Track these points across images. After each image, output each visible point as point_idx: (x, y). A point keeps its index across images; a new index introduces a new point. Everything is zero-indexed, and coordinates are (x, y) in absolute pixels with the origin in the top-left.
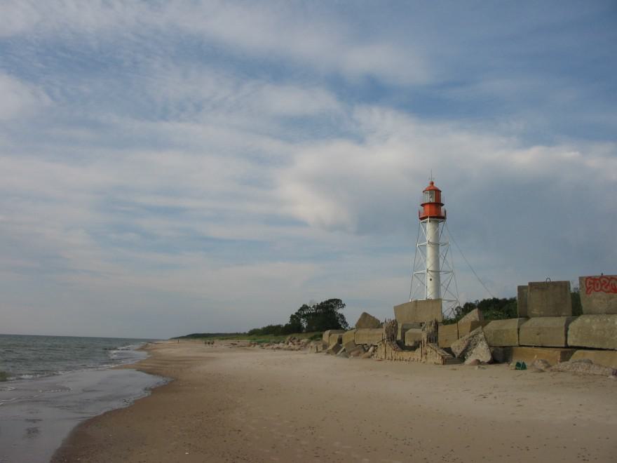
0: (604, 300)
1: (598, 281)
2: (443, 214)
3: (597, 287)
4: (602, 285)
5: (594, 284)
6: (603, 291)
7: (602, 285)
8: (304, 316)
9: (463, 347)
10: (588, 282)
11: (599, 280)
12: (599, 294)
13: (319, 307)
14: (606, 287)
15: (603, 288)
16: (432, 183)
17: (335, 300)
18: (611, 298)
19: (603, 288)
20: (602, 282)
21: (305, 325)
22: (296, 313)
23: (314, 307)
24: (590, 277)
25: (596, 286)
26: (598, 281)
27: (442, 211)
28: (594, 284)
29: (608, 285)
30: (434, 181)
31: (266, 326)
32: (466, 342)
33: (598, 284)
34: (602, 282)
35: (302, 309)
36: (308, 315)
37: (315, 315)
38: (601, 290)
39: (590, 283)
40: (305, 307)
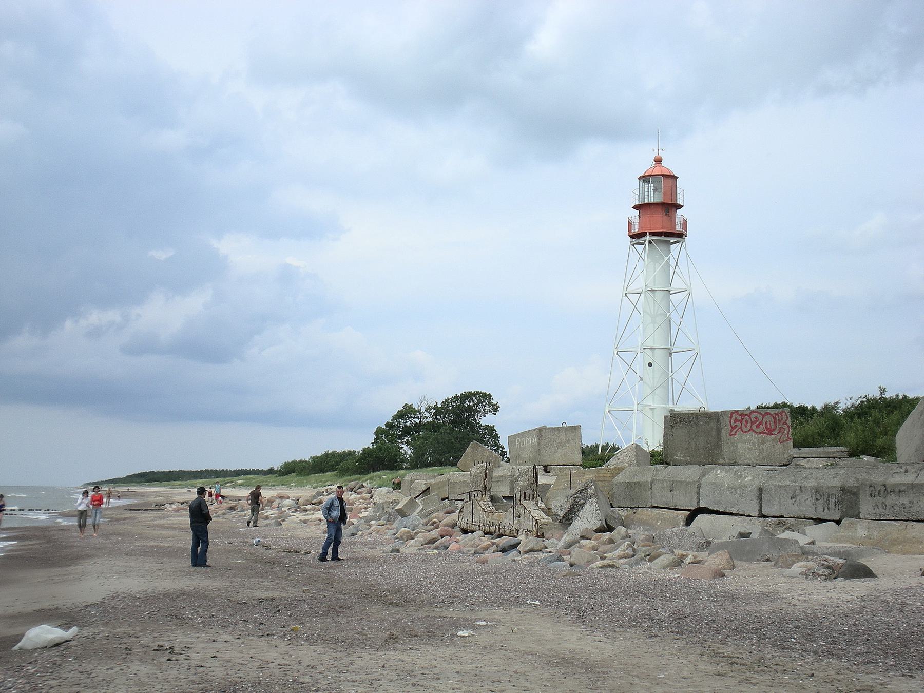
0: (754, 444)
1: (747, 418)
2: (679, 229)
3: (746, 426)
4: (752, 423)
5: (741, 421)
6: (754, 431)
7: (752, 423)
8: (407, 431)
9: (567, 507)
10: (734, 418)
11: (749, 416)
12: (747, 436)
13: (439, 411)
14: (758, 427)
15: (754, 427)
16: (658, 161)
17: (477, 394)
18: (763, 442)
19: (754, 427)
20: (753, 419)
21: (407, 450)
22: (387, 425)
23: (428, 409)
24: (737, 412)
25: (743, 424)
26: (747, 418)
27: (679, 219)
28: (741, 421)
29: (761, 423)
30: (662, 154)
31: (319, 453)
32: (571, 500)
33: (746, 421)
34: (753, 419)
35: (400, 415)
36: (418, 427)
37: (433, 427)
38: (751, 429)
39: (736, 420)
40: (407, 411)
